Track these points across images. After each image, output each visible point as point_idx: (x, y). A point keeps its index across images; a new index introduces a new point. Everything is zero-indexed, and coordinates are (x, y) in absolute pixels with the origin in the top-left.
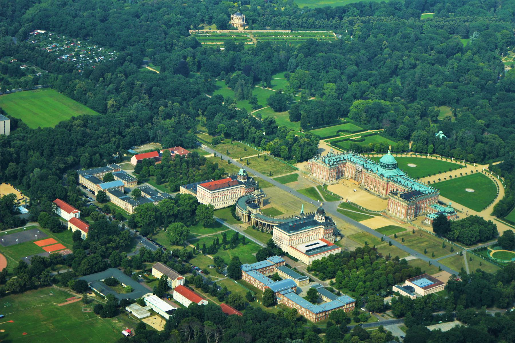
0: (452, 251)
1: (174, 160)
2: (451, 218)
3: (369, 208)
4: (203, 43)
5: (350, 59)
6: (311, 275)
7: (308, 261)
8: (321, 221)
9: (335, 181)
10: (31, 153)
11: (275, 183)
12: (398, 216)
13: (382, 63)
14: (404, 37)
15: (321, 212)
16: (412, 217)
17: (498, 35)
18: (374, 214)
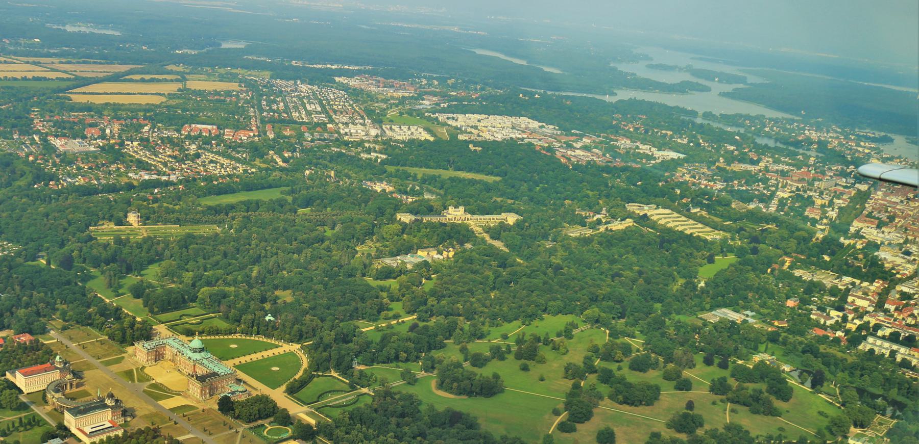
0: (231, 428)
2: (234, 398)
4: (99, 238)
5: (219, 250)
8: (110, 404)
9: (154, 363)
12: (195, 395)
13: (246, 252)
15: (111, 396)
17: (358, 227)
18: (176, 394)
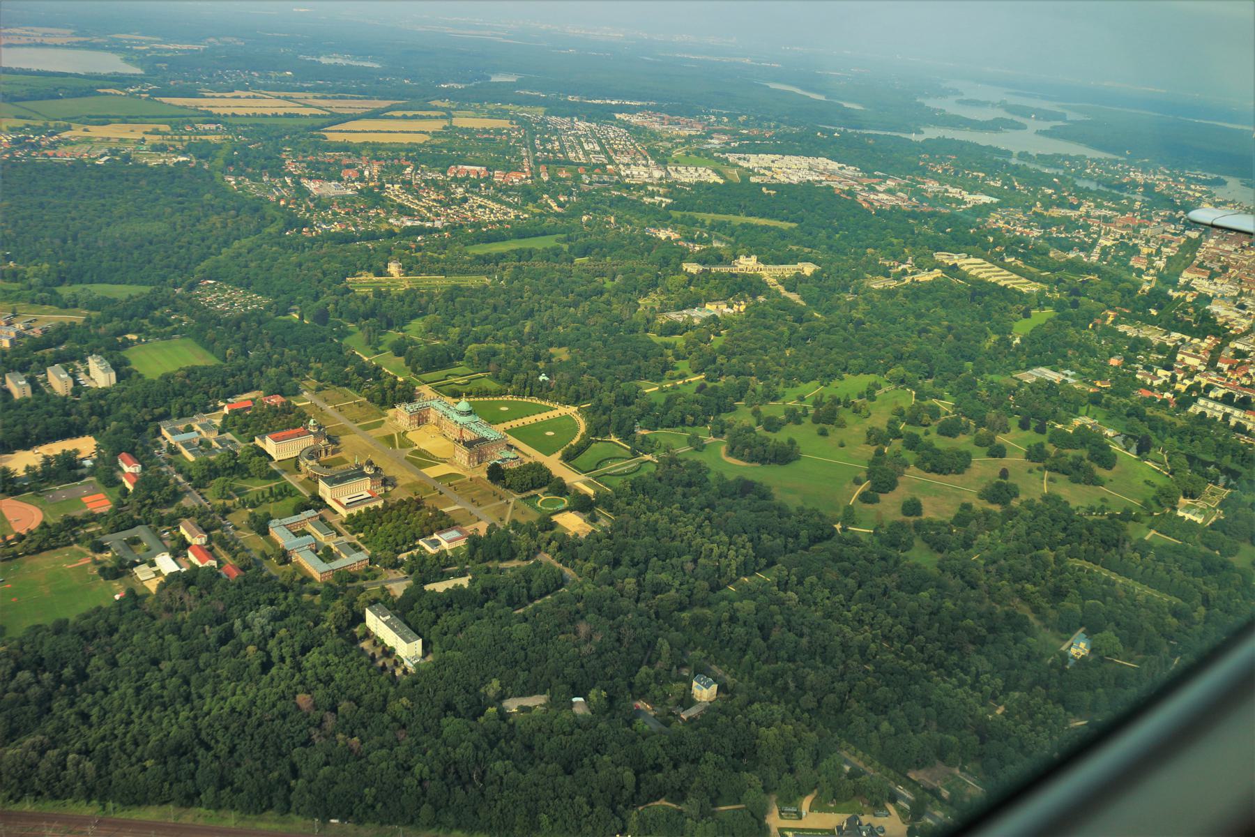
1: (1157, 214)
2: (505, 466)
3: (439, 455)
6: (342, 529)
7: (344, 513)
10: (124, 405)
11: (360, 430)
14: (549, 281)
15: (370, 463)
16: (476, 463)
